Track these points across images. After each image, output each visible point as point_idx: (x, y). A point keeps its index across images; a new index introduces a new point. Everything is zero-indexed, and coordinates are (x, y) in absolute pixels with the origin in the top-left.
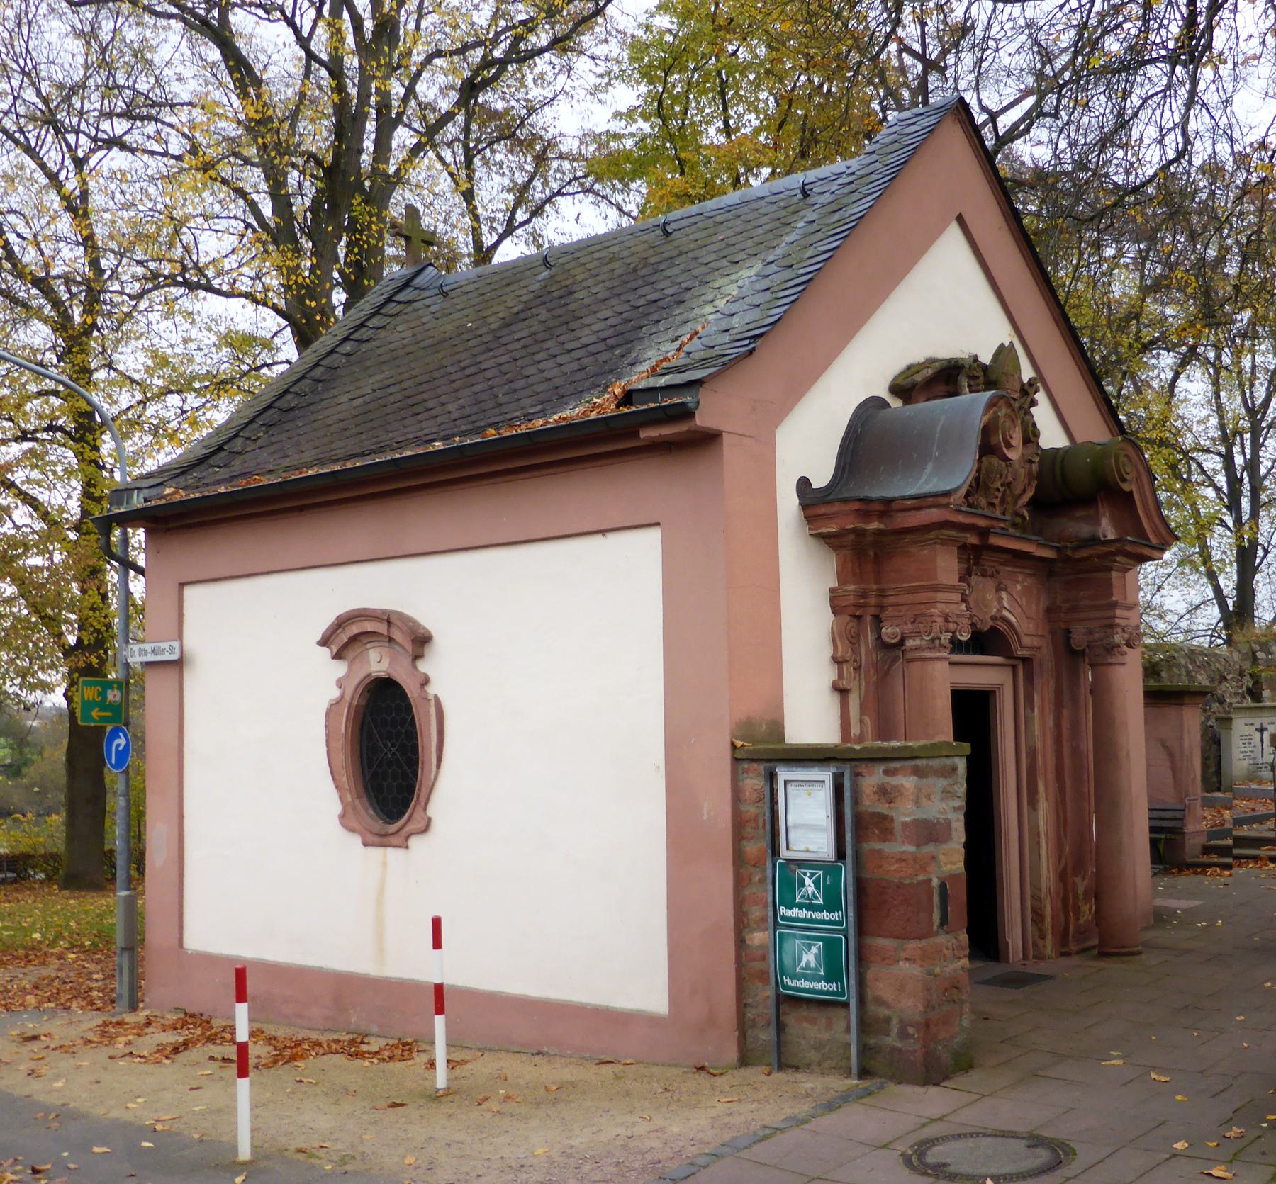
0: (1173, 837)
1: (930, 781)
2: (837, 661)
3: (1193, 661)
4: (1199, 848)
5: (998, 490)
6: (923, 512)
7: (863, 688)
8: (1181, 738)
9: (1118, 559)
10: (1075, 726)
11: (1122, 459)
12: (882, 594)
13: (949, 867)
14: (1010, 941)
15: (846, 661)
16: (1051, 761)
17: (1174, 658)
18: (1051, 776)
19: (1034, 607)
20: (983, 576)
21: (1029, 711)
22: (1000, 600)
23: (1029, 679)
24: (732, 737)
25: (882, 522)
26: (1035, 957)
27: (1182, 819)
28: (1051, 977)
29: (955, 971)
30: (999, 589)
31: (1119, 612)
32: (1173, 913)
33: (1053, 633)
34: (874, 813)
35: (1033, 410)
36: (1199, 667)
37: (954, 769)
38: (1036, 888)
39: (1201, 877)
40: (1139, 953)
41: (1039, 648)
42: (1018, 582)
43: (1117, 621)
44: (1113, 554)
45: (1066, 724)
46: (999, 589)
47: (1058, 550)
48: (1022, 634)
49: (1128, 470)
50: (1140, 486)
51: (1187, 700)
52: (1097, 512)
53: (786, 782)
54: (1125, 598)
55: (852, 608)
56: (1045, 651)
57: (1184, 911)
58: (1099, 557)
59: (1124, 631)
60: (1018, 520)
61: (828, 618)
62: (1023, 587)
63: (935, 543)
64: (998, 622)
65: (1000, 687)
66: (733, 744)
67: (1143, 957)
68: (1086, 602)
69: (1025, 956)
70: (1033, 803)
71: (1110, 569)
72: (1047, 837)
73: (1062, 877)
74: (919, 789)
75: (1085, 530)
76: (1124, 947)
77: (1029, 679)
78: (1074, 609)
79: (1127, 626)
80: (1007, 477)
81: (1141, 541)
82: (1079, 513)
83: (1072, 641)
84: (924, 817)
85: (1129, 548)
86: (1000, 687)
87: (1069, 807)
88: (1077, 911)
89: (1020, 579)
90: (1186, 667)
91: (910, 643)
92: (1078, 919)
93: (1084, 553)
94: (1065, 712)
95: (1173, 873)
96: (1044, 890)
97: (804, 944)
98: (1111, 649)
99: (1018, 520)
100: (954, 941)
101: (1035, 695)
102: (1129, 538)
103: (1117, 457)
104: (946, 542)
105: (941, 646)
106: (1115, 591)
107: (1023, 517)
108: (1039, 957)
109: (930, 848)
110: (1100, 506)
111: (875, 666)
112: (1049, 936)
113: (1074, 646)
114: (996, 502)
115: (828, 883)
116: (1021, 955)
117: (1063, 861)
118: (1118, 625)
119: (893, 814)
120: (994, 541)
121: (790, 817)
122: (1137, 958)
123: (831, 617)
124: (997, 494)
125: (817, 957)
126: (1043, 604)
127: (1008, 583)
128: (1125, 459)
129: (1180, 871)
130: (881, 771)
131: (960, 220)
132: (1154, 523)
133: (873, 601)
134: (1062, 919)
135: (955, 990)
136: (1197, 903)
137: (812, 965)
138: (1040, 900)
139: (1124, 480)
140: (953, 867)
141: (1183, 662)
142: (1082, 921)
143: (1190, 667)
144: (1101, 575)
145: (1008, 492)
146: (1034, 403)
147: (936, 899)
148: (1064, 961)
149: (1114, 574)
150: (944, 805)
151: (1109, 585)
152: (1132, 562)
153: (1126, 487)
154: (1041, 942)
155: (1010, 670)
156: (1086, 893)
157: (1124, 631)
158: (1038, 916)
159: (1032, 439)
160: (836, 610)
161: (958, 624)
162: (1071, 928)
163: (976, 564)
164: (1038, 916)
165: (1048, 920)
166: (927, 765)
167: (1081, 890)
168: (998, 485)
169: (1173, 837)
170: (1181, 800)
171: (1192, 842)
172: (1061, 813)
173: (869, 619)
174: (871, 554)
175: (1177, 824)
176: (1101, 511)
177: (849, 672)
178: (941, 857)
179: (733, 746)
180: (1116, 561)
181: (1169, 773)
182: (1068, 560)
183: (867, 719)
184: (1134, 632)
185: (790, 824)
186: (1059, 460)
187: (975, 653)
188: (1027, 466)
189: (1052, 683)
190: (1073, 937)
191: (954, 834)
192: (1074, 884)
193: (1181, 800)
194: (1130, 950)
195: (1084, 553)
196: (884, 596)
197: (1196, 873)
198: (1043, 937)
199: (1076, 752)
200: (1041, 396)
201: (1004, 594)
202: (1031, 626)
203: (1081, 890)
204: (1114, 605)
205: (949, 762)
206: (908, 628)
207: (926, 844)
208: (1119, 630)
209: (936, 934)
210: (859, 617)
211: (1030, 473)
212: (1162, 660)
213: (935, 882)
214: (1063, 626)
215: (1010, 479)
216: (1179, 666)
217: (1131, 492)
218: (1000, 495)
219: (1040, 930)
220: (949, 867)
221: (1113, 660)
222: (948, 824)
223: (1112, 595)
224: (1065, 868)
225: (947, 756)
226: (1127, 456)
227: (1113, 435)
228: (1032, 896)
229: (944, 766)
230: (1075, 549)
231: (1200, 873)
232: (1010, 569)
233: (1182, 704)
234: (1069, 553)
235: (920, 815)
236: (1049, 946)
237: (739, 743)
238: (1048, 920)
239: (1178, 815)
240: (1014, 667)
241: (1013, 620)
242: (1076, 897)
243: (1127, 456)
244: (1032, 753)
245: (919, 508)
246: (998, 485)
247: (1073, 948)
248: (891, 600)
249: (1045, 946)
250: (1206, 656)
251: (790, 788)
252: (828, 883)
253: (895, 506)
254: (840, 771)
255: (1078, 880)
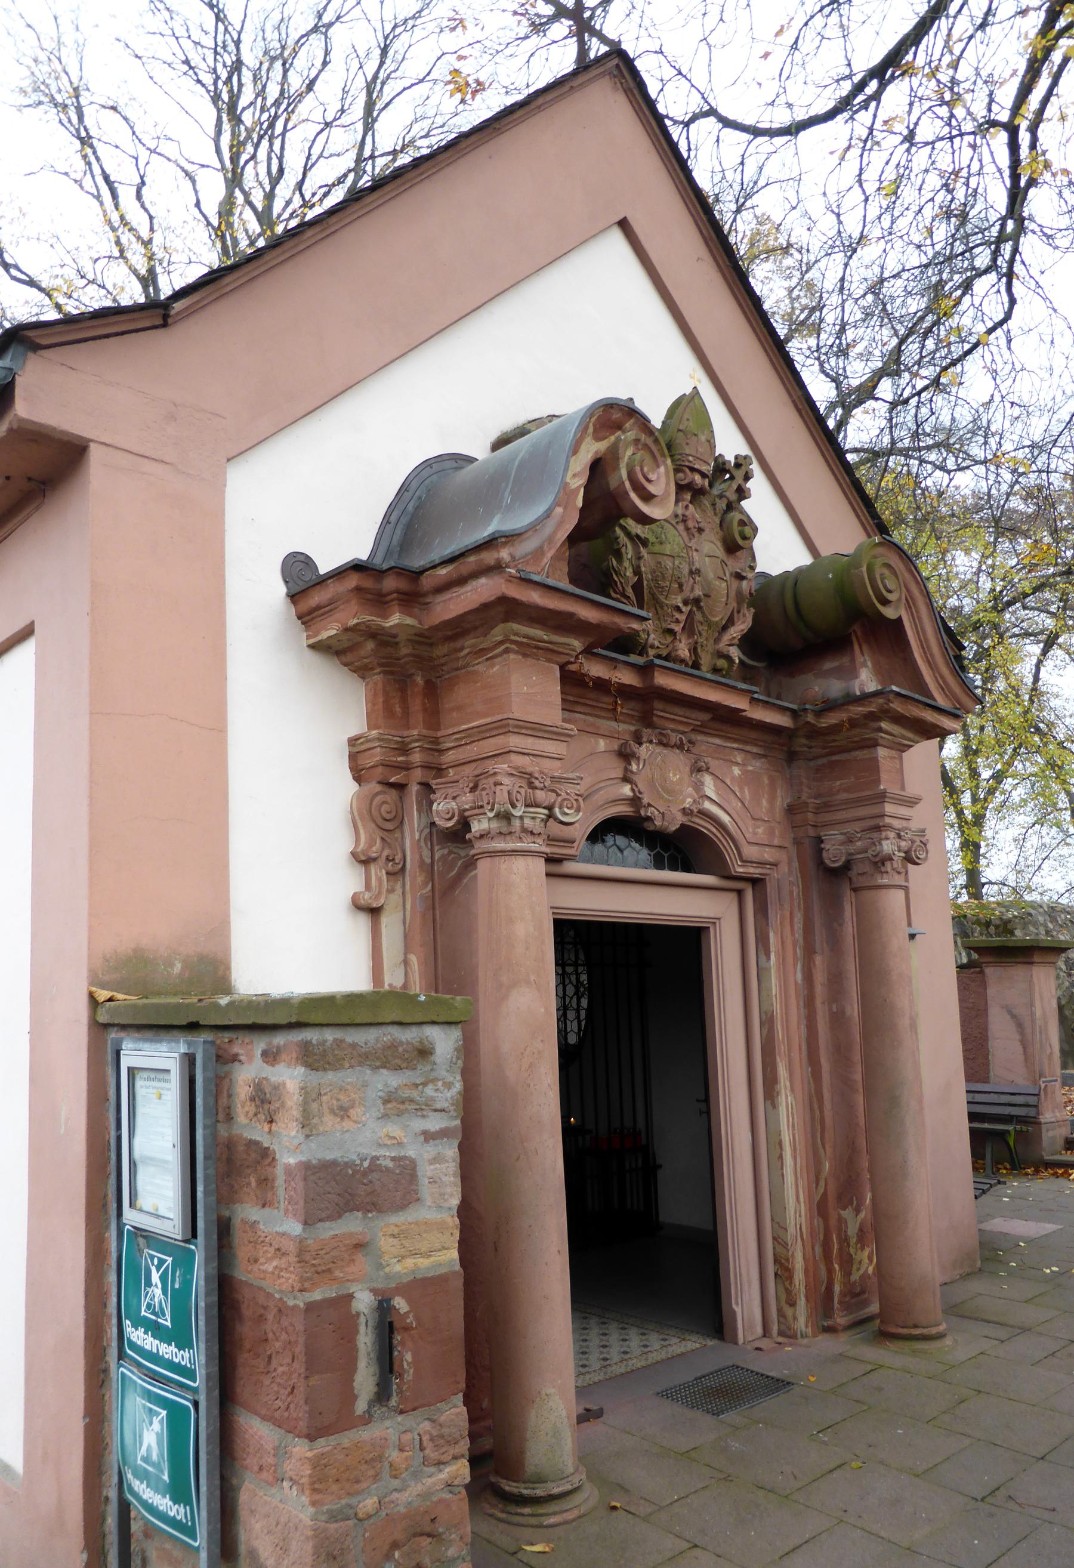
0: (1024, 1128)
1: (349, 1077)
2: (363, 860)
3: (1054, 920)
4: (1061, 1142)
5: (678, 609)
6: (468, 587)
7: (408, 906)
8: (1032, 1005)
9: (884, 725)
10: (836, 979)
11: (878, 571)
12: (435, 747)
13: (410, 1262)
14: (738, 1310)
15: (375, 860)
16: (798, 1032)
17: (1030, 915)
18: (799, 1056)
19: (765, 803)
20: (661, 743)
21: (763, 957)
22: (698, 786)
23: (762, 910)
24: (91, 984)
25: (410, 615)
26: (781, 1333)
27: (1036, 1106)
28: (779, 1385)
29: (424, 1496)
30: (697, 769)
31: (889, 808)
32: (1012, 1243)
33: (797, 842)
34: (250, 1140)
35: (743, 503)
36: (1061, 926)
37: (424, 1052)
38: (780, 1226)
39: (1062, 1181)
40: (940, 1336)
41: (775, 865)
42: (737, 764)
43: (887, 820)
44: (872, 717)
45: (820, 978)
46: (697, 769)
47: (794, 714)
48: (742, 842)
49: (891, 585)
50: (911, 603)
51: (1036, 958)
52: (853, 660)
53: (131, 1071)
54: (903, 788)
55: (380, 769)
56: (784, 868)
57: (1029, 1241)
58: (853, 723)
59: (899, 836)
60: (722, 663)
61: (345, 788)
62: (745, 772)
63: (507, 651)
64: (697, 820)
65: (715, 921)
66: (91, 996)
67: (948, 1341)
68: (844, 796)
69: (766, 1332)
70: (771, 1094)
71: (874, 744)
72: (794, 1150)
73: (821, 1209)
74: (310, 1097)
75: (835, 688)
76: (916, 1326)
77: (762, 910)
78: (825, 807)
79: (904, 829)
80: (692, 589)
81: (917, 696)
82: (828, 665)
83: (825, 854)
84: (329, 1156)
85: (897, 706)
86: (715, 921)
87: (827, 1105)
88: (847, 1262)
89: (739, 759)
90: (1046, 926)
91: (477, 826)
92: (848, 1274)
93: (832, 719)
94: (818, 959)
95: (1027, 1174)
96: (791, 1230)
97: (144, 1406)
98: (881, 862)
99: (722, 663)
100: (426, 1425)
101: (772, 935)
102: (894, 688)
103: (870, 570)
104: (529, 649)
105: (524, 830)
106: (884, 776)
107: (728, 658)
108: (788, 1334)
109: (352, 1225)
110: (856, 647)
111: (429, 870)
112: (802, 1302)
113: (827, 861)
114: (677, 628)
115: (177, 1286)
116: (759, 1330)
117: (822, 1183)
118: (889, 827)
119: (275, 1147)
120: (662, 680)
121: (137, 1141)
122: (937, 1344)
123: (353, 787)
124: (677, 615)
125: (159, 1436)
126: (782, 800)
127: (714, 764)
128: (886, 572)
129: (1037, 1172)
130: (258, 1053)
131: (624, 225)
132: (942, 677)
133: (417, 757)
134: (823, 1272)
135: (425, 1541)
136: (1049, 1227)
137: (155, 1457)
138: (785, 1246)
139: (885, 602)
140: (424, 1263)
141: (1041, 919)
142: (855, 1277)
143: (1050, 926)
144: (860, 754)
145: (698, 616)
146: (742, 493)
147: (365, 1340)
148: (827, 1345)
149: (882, 752)
150: (394, 1129)
151: (873, 767)
152: (910, 735)
153: (890, 613)
154: (789, 1311)
155: (732, 897)
156: (861, 1231)
157: (899, 836)
158: (784, 1271)
159: (740, 542)
160: (359, 774)
161: (558, 795)
162: (837, 1288)
163: (650, 725)
164: (784, 1271)
165: (799, 1276)
166: (339, 1043)
167: (852, 1230)
168: (678, 601)
169: (1024, 1128)
170: (1035, 1082)
171: (1051, 1134)
172: (817, 1113)
173: (414, 788)
174: (419, 680)
175: (1032, 1112)
176: (859, 659)
177: (379, 880)
178: (385, 1244)
179: (94, 1002)
180: (880, 730)
181: (1019, 1049)
182: (814, 733)
183: (413, 959)
184: (917, 839)
185: (137, 1155)
186: (790, 584)
187: (673, 868)
188: (735, 584)
189: (799, 917)
190: (840, 1302)
191: (426, 1190)
192: (841, 1220)
193: (1035, 1082)
194: (925, 1331)
195: (832, 719)
196: (441, 752)
197: (1056, 1175)
198: (792, 1304)
199: (838, 1019)
200: (758, 484)
201: (708, 780)
202: (760, 831)
203: (852, 1230)
204: (881, 797)
205: (409, 1036)
206: (467, 800)
207: (336, 1215)
208: (892, 835)
209: (367, 1419)
210: (400, 787)
211: (739, 594)
212: (1015, 917)
213: (364, 1301)
214: (811, 832)
215: (698, 592)
216: (1036, 924)
217: (900, 619)
218: (682, 618)
219: (788, 1292)
220: (410, 1262)
221: (885, 881)
222: (407, 1170)
223: (878, 781)
224: (825, 1195)
225: (400, 1024)
226: (888, 566)
227: (869, 536)
228: (774, 1238)
229: (393, 1046)
230: (819, 714)
231: (1062, 1175)
232: (718, 741)
233: (1032, 963)
234: (810, 718)
235: (318, 1151)
236: (801, 1317)
237: (103, 995)
238: (799, 1276)
239: (1032, 1100)
240: (740, 893)
241: (725, 818)
242: (844, 1240)
243: (888, 566)
244: (768, 1022)
245: (461, 581)
246: (678, 601)
247: (841, 1320)
248: (450, 757)
249: (795, 1318)
250: (1069, 913)
251: (139, 1083)
252: (177, 1286)
253: (427, 582)
254: (191, 1051)
255: (847, 1214)
